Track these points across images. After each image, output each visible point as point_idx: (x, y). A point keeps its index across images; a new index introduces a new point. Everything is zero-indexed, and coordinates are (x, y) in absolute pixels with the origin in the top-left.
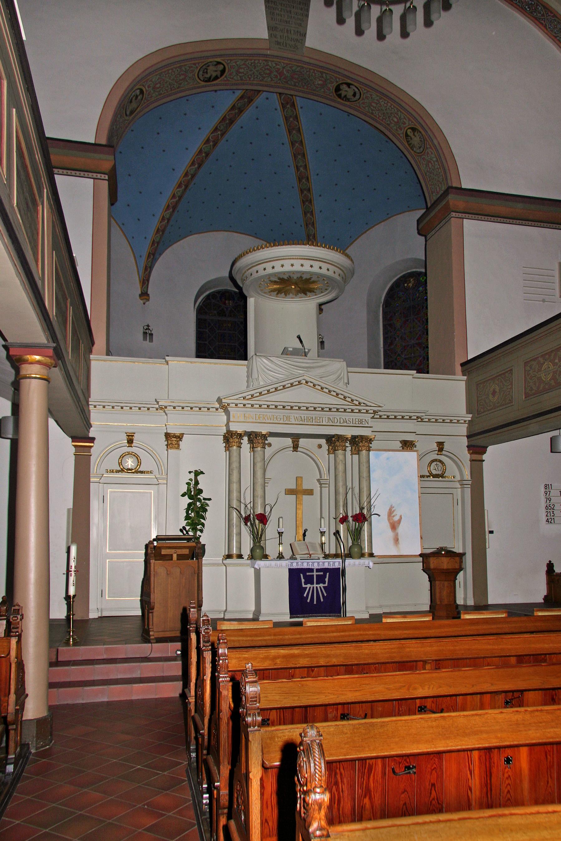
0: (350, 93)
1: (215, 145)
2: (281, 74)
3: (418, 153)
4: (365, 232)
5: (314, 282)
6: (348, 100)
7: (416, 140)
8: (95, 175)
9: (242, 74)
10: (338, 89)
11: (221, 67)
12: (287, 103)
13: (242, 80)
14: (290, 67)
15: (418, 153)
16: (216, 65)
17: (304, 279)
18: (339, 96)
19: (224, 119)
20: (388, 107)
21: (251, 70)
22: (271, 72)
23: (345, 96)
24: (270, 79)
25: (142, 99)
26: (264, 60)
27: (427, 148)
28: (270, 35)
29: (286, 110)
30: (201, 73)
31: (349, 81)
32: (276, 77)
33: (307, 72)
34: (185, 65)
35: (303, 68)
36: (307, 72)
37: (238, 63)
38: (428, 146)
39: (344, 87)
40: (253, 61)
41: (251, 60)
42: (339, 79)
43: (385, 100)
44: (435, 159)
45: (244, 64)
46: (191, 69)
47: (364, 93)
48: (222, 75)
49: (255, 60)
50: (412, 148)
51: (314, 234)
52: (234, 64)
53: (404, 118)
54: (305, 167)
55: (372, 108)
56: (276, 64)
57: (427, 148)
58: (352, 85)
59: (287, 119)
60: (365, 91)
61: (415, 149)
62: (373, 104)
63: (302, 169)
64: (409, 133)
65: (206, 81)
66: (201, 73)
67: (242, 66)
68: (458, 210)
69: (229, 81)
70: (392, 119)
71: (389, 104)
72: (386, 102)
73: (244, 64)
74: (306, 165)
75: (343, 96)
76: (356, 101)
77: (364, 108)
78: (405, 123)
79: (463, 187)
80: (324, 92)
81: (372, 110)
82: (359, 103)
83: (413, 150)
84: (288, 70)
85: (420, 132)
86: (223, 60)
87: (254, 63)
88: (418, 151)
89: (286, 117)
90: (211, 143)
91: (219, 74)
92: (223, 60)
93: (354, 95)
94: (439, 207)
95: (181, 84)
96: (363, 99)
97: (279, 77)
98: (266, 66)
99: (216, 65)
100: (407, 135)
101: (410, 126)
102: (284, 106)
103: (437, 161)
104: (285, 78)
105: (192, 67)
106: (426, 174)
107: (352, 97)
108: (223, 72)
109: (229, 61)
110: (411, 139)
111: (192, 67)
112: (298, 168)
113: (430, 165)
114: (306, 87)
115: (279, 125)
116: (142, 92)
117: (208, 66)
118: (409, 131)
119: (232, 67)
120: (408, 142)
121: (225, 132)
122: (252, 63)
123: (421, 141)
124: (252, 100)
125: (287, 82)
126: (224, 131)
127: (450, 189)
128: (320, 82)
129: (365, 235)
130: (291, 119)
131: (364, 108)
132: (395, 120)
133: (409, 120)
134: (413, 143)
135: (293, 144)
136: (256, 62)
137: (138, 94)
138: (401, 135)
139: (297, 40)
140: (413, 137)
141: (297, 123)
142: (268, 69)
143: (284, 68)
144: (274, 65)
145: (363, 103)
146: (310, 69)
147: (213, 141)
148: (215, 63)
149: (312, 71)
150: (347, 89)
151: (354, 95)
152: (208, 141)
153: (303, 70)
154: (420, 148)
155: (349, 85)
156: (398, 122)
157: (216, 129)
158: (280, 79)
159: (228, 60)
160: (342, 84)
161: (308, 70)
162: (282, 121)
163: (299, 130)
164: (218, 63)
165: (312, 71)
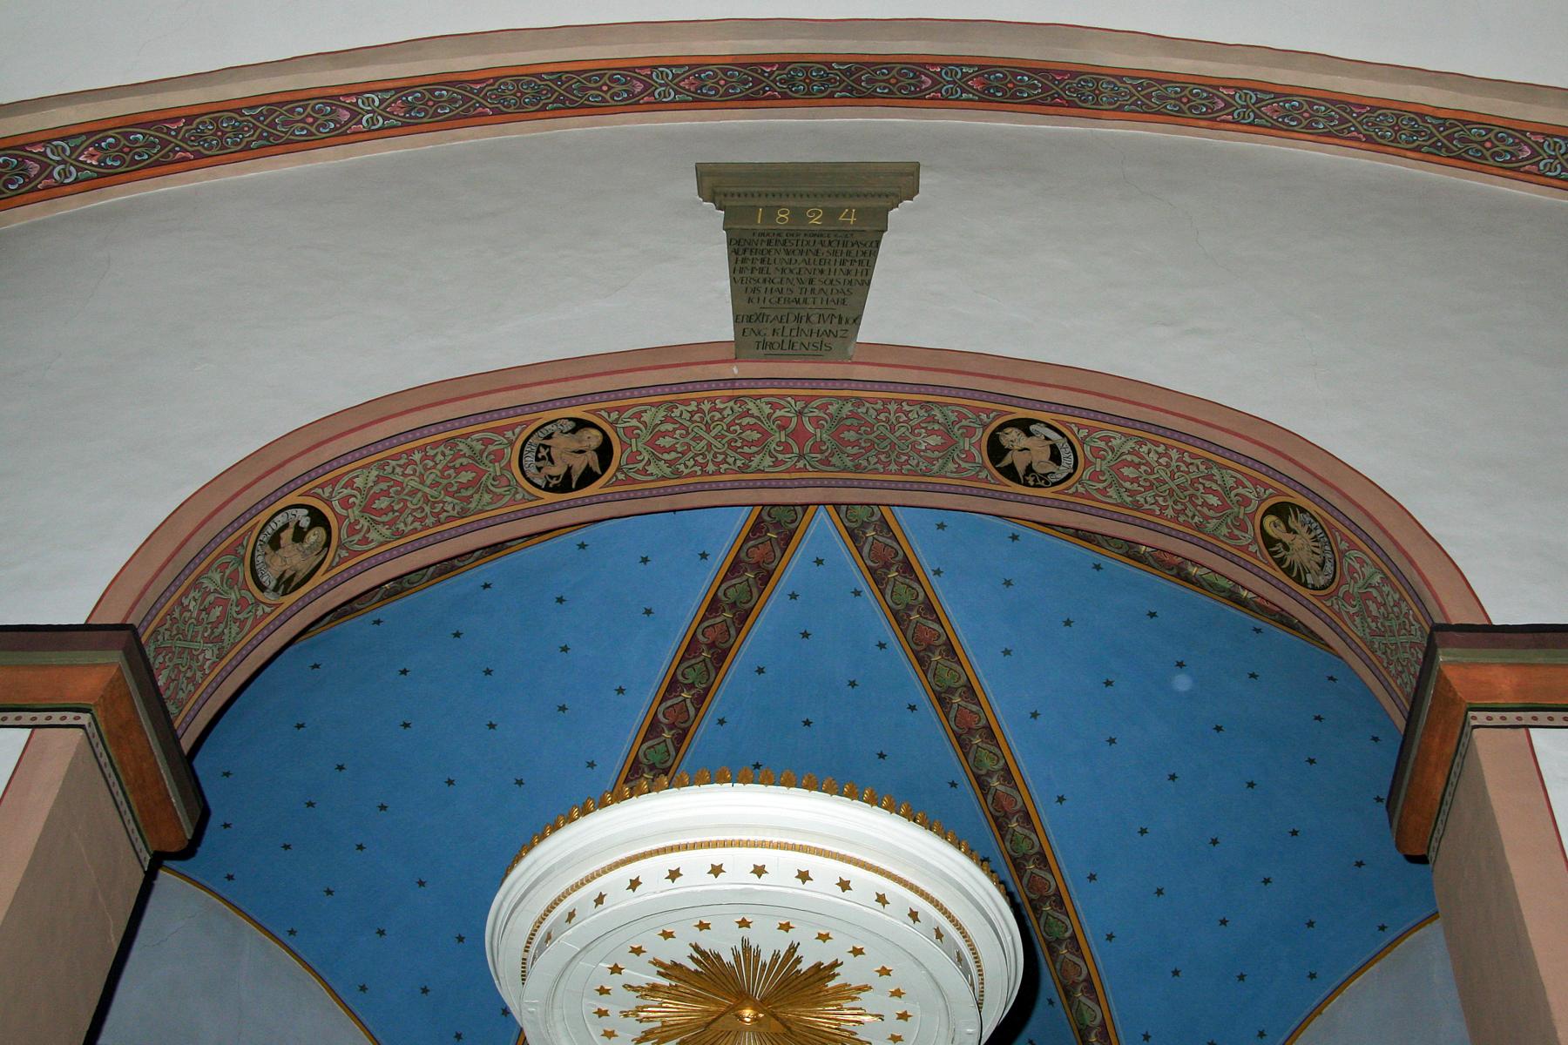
0: (1039, 456)
1: (680, 739)
2: (799, 435)
3: (1323, 588)
4: (1317, 1010)
5: (847, 993)
6: (1043, 481)
7: (1301, 547)
8: (27, 717)
9: (673, 455)
10: (996, 450)
11: (592, 438)
12: (887, 566)
13: (678, 474)
14: (824, 407)
15: (1323, 588)
16: (573, 431)
17: (766, 957)
18: (1010, 472)
19: (692, 648)
20: (1174, 464)
21: (699, 438)
22: (766, 434)
23: (1029, 469)
24: (768, 461)
25: (328, 544)
26: (730, 398)
27: (1343, 553)
28: (740, 332)
29: (888, 592)
30: (529, 459)
31: (1021, 413)
32: (787, 449)
33: (879, 412)
34: (468, 436)
35: (860, 402)
36: (879, 412)
37: (646, 417)
38: (1344, 546)
39: (1012, 437)
40: (693, 406)
41: (686, 402)
42: (987, 411)
43: (1157, 444)
44: (1377, 579)
45: (667, 419)
46: (491, 448)
47: (1082, 442)
48: (605, 465)
49: (700, 401)
50: (1298, 580)
51: (1103, 1025)
52: (634, 422)
53: (1239, 483)
54: (1007, 776)
55: (1127, 485)
56: (774, 406)
57: (1343, 553)
58: (1034, 422)
59: (899, 618)
60: (1084, 433)
61: (1310, 579)
62: (1126, 471)
63: (995, 783)
64: (1270, 530)
65: (555, 490)
66: (529, 459)
67: (663, 428)
68: (1501, 702)
69: (635, 481)
70: (1205, 504)
71: (1174, 454)
72: (1161, 449)
73: (667, 419)
74: (1007, 769)
75: (1021, 469)
76: (1069, 476)
77: (1103, 492)
78: (1245, 502)
79: (1497, 620)
80: (959, 470)
81: (1132, 493)
82: (1080, 481)
83: (1305, 585)
84: (818, 418)
85: (1303, 511)
86: (594, 412)
87: (700, 410)
88: (1322, 581)
89: (895, 614)
90: (667, 735)
91: (592, 459)
92: (594, 412)
93: (1056, 457)
94: (1428, 702)
95: (468, 499)
96: (1088, 463)
97: (796, 450)
98: (741, 417)
99: (573, 431)
100: (1269, 542)
101: (1265, 506)
102: (878, 579)
103: (1386, 579)
104: (816, 448)
105: (491, 441)
106: (1370, 646)
107: (1052, 467)
108: (605, 452)
109: (614, 415)
110: (1286, 548)
111: (491, 441)
112: (982, 783)
113: (1373, 607)
114: (893, 467)
115: (882, 646)
116: (318, 519)
117: (549, 437)
118: (1272, 526)
119: (629, 431)
120: (1280, 562)
121: (707, 690)
122: (692, 413)
123: (1315, 539)
124: (770, 574)
125: (826, 462)
126: (700, 686)
127: (1441, 632)
128: (934, 440)
129: (1318, 1022)
130: (914, 616)
131: (1103, 492)
132: (1213, 500)
133: (1256, 482)
134: (1295, 557)
135: (942, 700)
136: (706, 406)
137: (305, 523)
138: (1253, 548)
139: (829, 333)
140: (1287, 538)
141: (936, 626)
142: (751, 427)
143: (800, 413)
144: (767, 410)
145: (1095, 476)
146: (886, 401)
147: (672, 727)
148: (571, 425)
149: (893, 407)
150: (1024, 441)
151: (1056, 457)
152: (653, 729)
153: (863, 410)
154: (1322, 565)
155: (1024, 426)
156: (1225, 506)
157: (673, 686)
158: (801, 456)
159: (609, 411)
160: (1002, 427)
161: (879, 406)
162: (885, 629)
163: (950, 651)
164: (580, 424)
165: (893, 407)
